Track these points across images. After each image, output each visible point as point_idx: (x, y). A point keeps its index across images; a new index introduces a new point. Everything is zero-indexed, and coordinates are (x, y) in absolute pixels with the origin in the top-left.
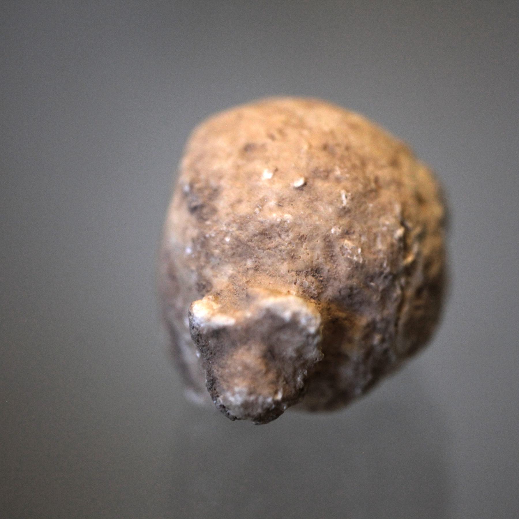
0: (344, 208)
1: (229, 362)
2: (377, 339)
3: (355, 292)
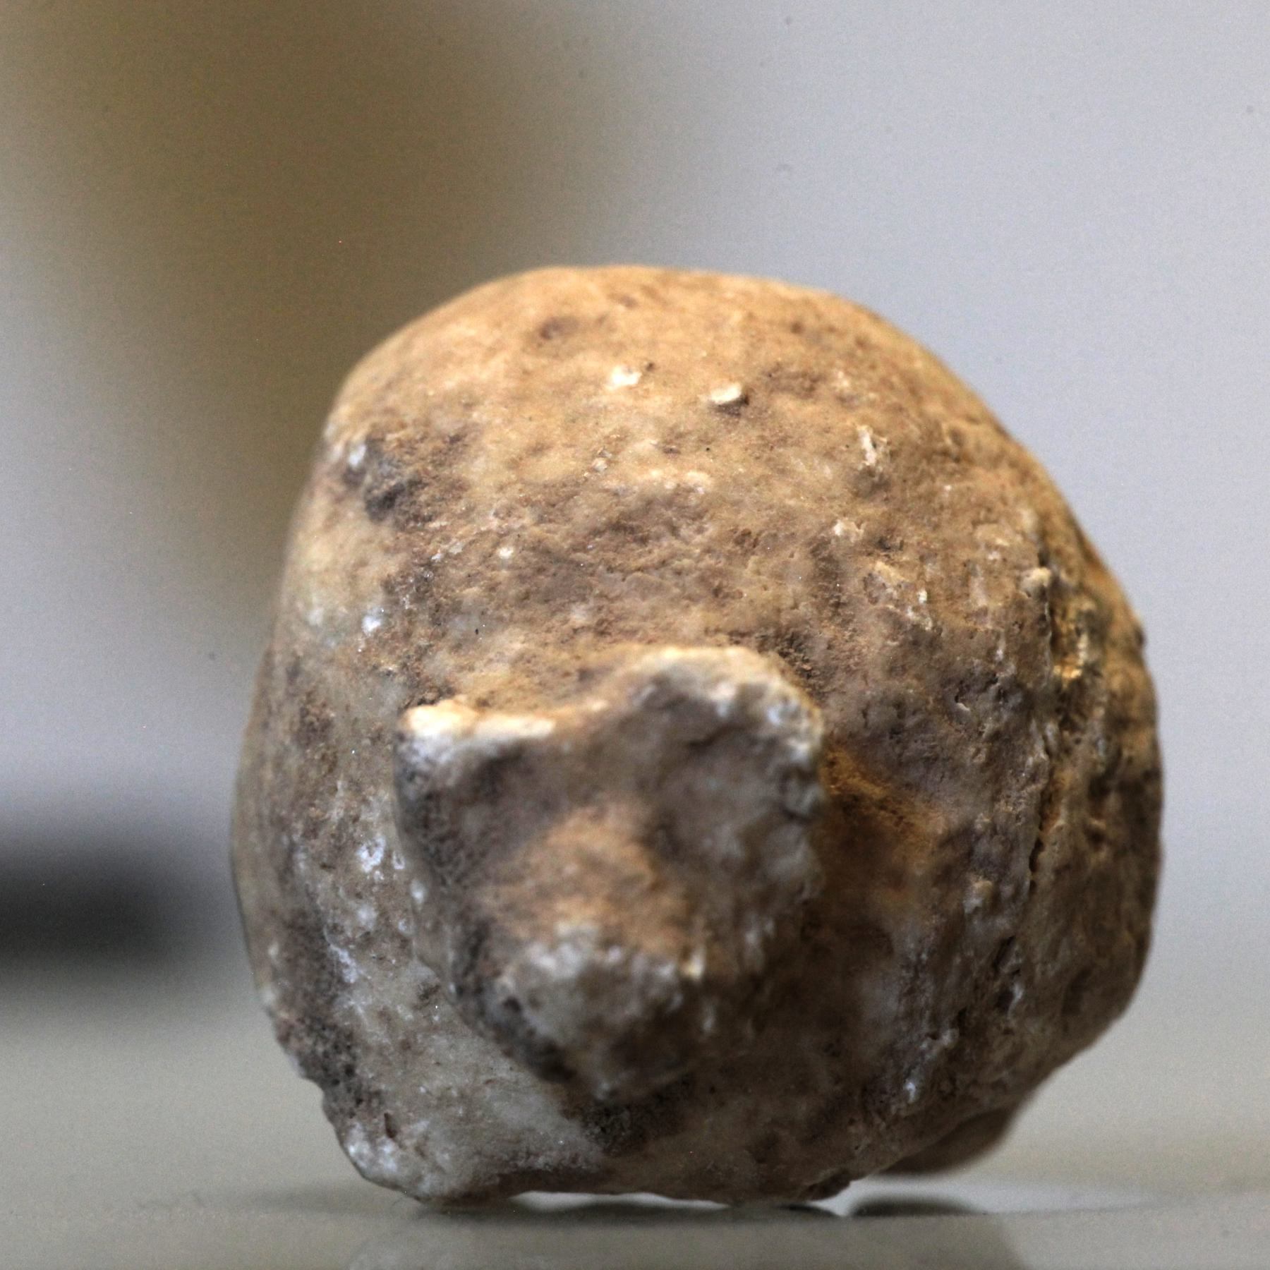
0: (869, 472)
1: (534, 860)
2: (978, 888)
3: (911, 722)
